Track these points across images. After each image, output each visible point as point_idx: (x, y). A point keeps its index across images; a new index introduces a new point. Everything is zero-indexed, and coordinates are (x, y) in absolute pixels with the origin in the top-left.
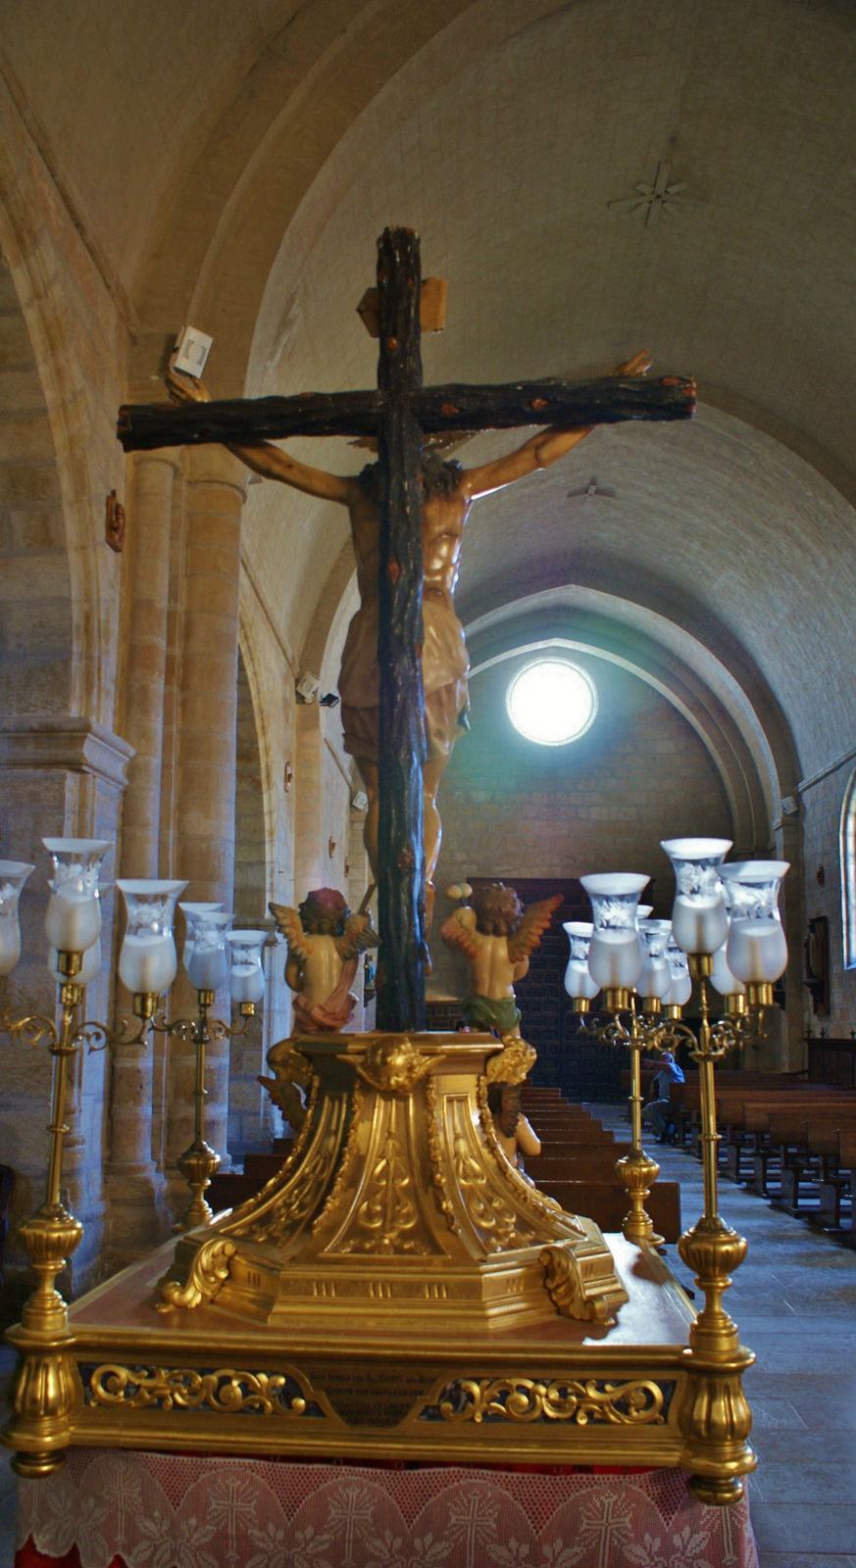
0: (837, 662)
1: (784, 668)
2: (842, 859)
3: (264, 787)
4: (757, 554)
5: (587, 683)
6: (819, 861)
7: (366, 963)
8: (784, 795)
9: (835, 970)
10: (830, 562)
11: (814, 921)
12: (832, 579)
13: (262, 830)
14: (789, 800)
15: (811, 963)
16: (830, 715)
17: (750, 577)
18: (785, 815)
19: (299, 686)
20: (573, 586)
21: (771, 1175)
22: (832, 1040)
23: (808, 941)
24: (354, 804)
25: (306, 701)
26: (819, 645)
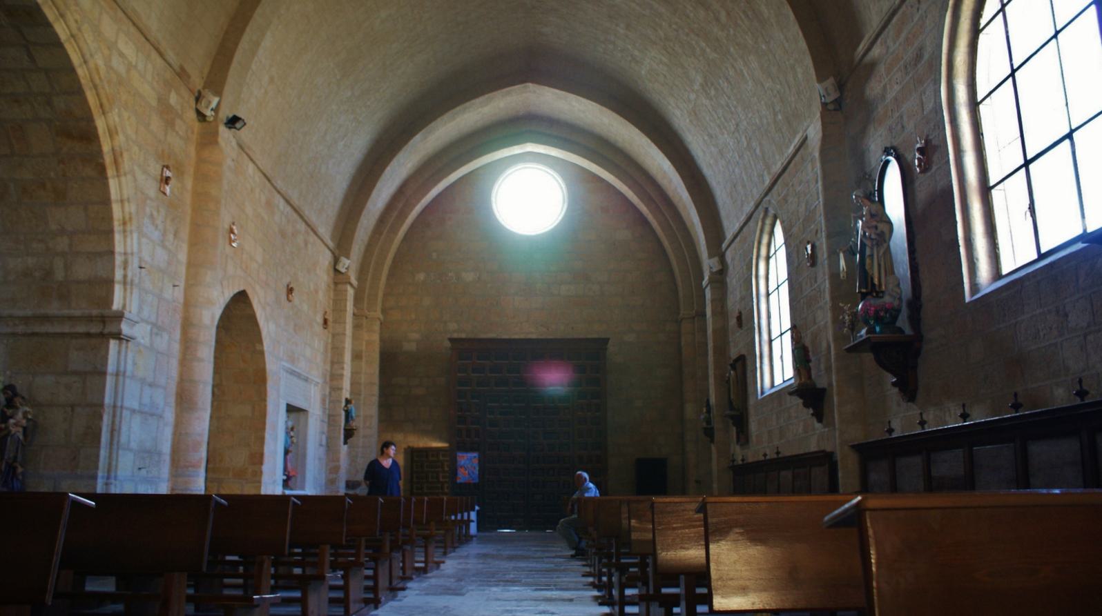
0: (743, 118)
1: (703, 139)
2: (755, 300)
3: (110, 172)
4: (670, 26)
5: (559, 183)
6: (738, 307)
7: (346, 406)
8: (711, 256)
9: (751, 402)
10: (728, 14)
11: (736, 360)
12: (732, 31)
13: (111, 219)
14: (716, 259)
15: (732, 397)
16: (742, 172)
17: (668, 53)
18: (711, 272)
19: (199, 104)
20: (530, 84)
21: (635, 567)
22: (750, 463)
23: (729, 378)
24: (337, 267)
25: (208, 119)
26: (728, 106)
